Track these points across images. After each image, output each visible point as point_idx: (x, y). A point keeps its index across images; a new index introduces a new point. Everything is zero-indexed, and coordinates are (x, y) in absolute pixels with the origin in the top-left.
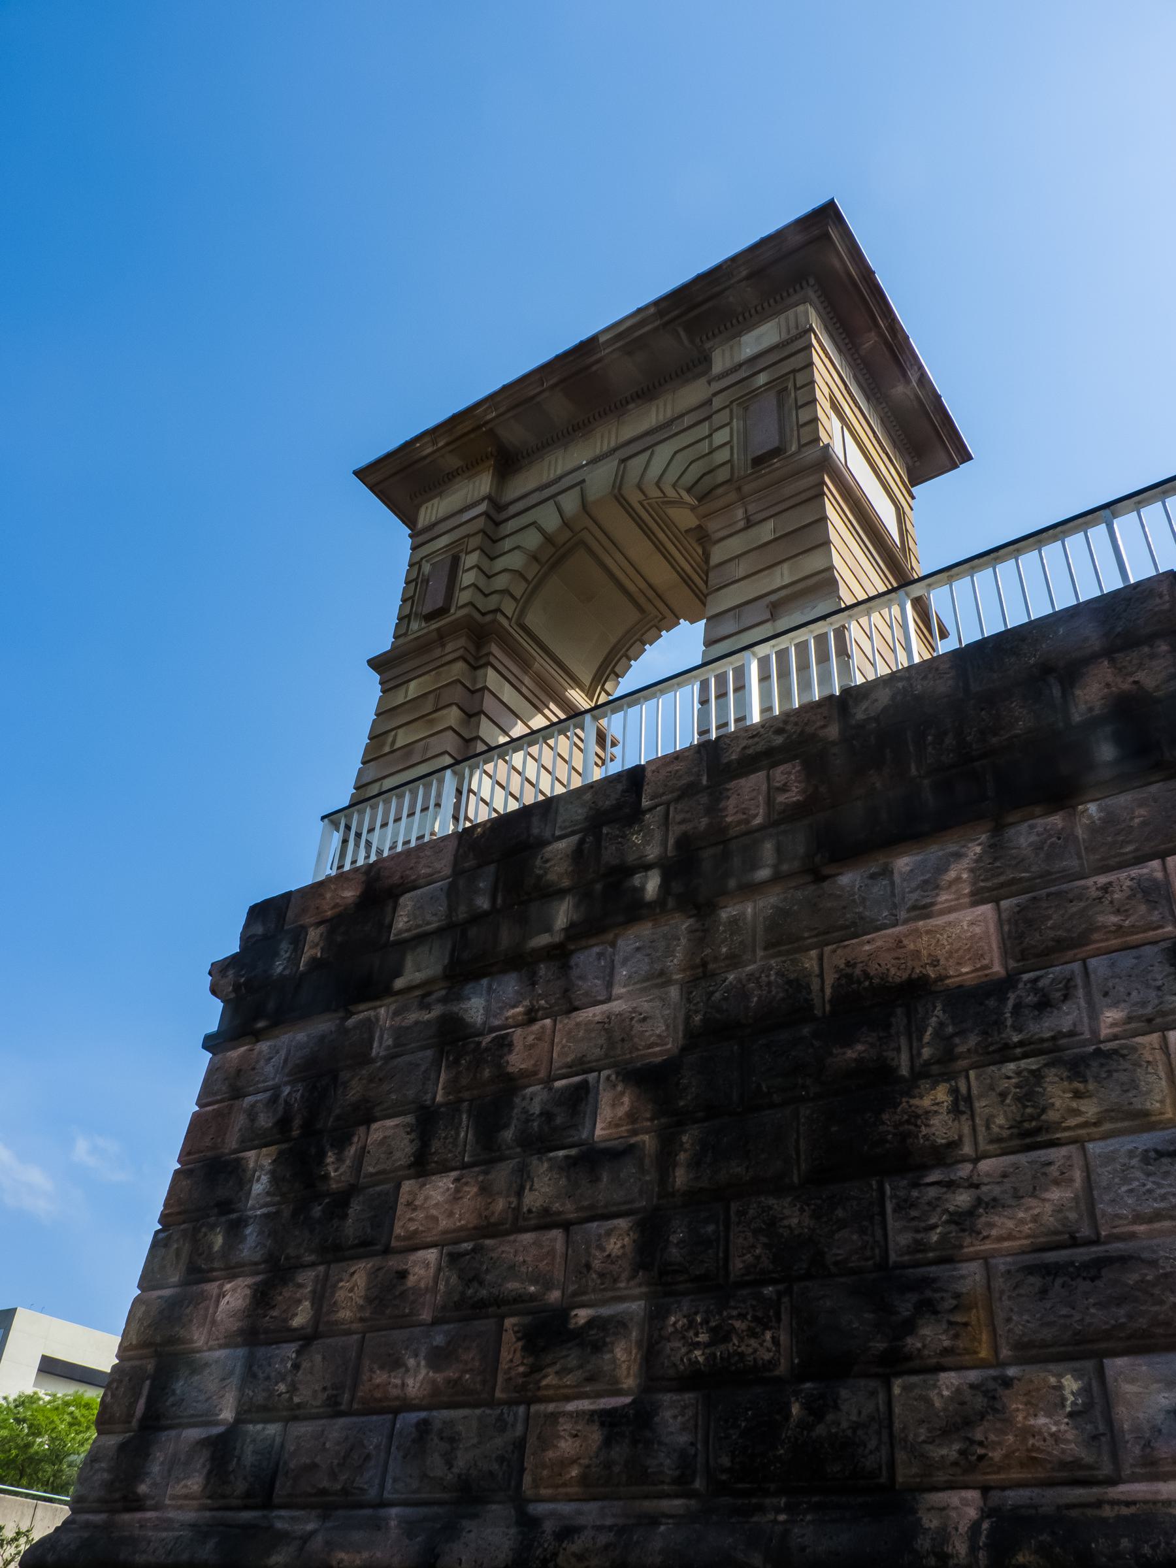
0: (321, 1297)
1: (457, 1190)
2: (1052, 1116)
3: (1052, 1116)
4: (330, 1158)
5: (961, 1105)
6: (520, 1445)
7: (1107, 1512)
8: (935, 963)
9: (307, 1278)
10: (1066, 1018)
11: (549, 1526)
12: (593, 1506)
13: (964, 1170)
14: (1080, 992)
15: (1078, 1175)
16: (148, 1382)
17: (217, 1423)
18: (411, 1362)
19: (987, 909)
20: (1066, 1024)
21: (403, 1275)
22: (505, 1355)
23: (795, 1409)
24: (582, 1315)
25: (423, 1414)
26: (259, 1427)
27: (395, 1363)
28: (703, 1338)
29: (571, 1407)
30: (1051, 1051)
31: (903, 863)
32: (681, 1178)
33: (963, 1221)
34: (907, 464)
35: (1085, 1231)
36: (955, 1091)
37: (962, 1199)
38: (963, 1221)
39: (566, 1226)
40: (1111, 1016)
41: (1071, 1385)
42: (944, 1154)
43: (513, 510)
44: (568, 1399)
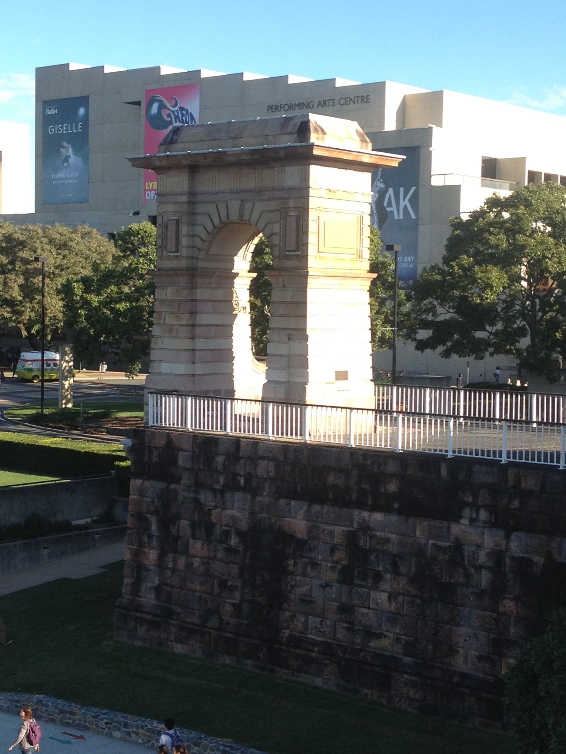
0: (174, 561)
1: (202, 547)
2: (307, 573)
3: (307, 573)
4: (171, 527)
5: (295, 564)
6: (219, 605)
7: (304, 639)
8: (295, 532)
9: (171, 556)
10: (313, 554)
11: (225, 621)
12: (232, 619)
13: (294, 578)
14: (317, 524)
15: (310, 585)
16: (135, 569)
17: (155, 583)
18: (196, 583)
19: (306, 522)
20: (313, 555)
21: (192, 563)
22: (215, 588)
23: (265, 612)
24: (229, 583)
25: (200, 594)
26: (165, 587)
27: (193, 582)
28: (250, 595)
29: (228, 601)
30: (313, 522)
31: (293, 503)
32: (247, 561)
33: (293, 587)
34: (229, 155)
35: (309, 595)
36: (295, 561)
37: (293, 583)
38: (293, 587)
39: (226, 563)
40: (320, 557)
41: (303, 619)
42: (292, 574)
43: (348, 433)
44: (228, 599)
